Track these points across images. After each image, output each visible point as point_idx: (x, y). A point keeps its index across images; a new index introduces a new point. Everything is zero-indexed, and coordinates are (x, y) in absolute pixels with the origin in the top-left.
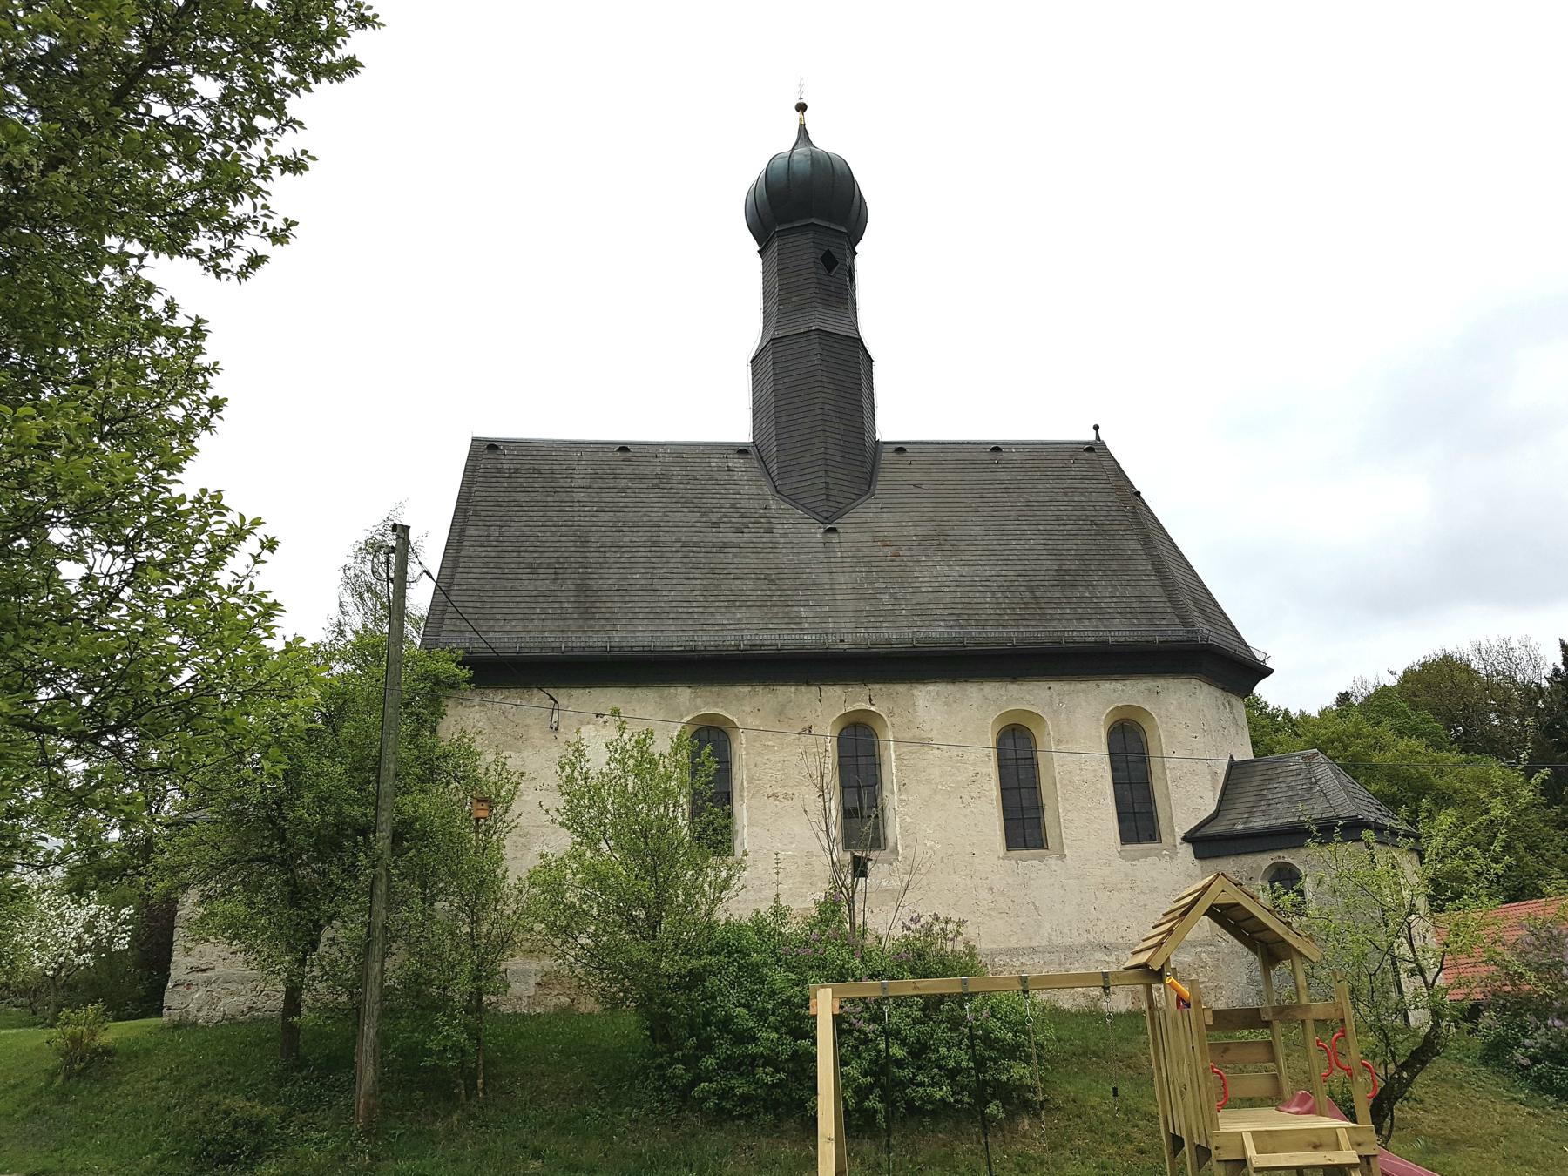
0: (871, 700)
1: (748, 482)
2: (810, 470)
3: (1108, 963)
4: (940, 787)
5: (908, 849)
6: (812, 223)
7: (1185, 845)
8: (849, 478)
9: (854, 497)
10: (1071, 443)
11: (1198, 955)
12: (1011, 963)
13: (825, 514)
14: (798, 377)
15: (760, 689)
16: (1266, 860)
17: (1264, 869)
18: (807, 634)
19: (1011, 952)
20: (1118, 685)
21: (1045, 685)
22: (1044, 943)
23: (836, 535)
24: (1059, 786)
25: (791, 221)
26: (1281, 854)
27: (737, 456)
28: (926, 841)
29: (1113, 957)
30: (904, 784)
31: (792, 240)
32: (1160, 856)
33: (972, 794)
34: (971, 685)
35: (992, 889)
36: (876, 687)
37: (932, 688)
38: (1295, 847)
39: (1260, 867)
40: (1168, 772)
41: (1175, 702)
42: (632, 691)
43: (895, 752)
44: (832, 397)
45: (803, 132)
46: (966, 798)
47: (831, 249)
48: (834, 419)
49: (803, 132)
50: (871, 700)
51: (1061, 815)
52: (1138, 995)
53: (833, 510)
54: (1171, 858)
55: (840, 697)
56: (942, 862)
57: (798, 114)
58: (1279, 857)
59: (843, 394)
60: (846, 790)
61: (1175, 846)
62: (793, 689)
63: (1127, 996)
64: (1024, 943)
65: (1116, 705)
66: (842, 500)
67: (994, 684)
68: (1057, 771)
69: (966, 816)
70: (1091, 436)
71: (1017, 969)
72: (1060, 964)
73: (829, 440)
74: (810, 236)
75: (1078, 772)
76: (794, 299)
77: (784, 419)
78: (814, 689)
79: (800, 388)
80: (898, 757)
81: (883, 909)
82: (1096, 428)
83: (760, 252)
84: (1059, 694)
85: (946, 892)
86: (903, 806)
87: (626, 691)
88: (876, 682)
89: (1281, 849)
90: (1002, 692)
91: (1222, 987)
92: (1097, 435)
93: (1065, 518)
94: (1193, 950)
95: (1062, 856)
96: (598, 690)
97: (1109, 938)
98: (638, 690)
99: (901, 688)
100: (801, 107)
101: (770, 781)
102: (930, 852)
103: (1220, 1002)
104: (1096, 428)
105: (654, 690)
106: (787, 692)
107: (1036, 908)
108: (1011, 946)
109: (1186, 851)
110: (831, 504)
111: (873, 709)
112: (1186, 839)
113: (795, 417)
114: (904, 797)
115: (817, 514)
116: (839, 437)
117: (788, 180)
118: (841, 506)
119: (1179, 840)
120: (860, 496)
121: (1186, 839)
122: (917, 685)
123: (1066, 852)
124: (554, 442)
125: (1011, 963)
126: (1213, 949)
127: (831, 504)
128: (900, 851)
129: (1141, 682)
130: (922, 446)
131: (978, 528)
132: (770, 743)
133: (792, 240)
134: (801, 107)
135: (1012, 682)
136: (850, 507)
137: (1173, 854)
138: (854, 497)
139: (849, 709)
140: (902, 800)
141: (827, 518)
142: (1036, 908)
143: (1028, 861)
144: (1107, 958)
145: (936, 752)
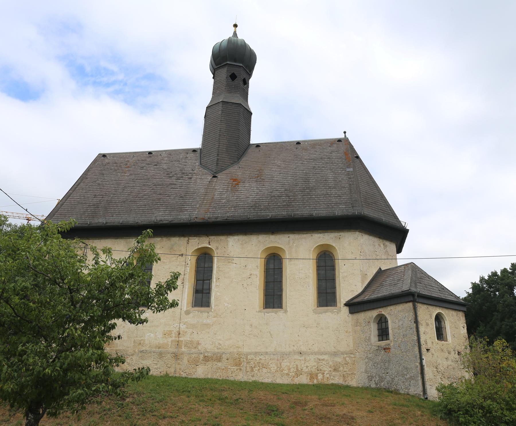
0: (209, 243)
1: (194, 161)
2: (212, 155)
3: (300, 360)
4: (234, 280)
5: (217, 307)
6: (227, 64)
7: (345, 307)
8: (229, 157)
9: (230, 164)
10: (332, 139)
11: (345, 358)
12: (255, 358)
13: (215, 171)
14: (214, 120)
15: (165, 239)
16: (374, 313)
17: (374, 317)
18: (184, 217)
19: (256, 354)
20: (321, 235)
21: (287, 236)
22: (273, 350)
23: (216, 178)
24: (288, 280)
25: (221, 64)
26: (380, 310)
27: (192, 153)
28: (225, 303)
29: (303, 358)
30: (219, 279)
31: (220, 71)
32: (332, 312)
33: (248, 283)
34: (253, 236)
35: (251, 325)
36: (212, 238)
37: (236, 238)
38: (386, 306)
39: (372, 316)
40: (341, 274)
41: (347, 243)
42: (116, 240)
43: (217, 265)
44: (225, 126)
45: (235, 34)
46: (245, 285)
47: (235, 72)
48: (224, 134)
49: (235, 34)
50: (209, 243)
51: (288, 293)
52: (313, 375)
53: (219, 169)
54: (338, 313)
55: (196, 242)
56: (231, 313)
57: (233, 28)
58: (380, 312)
59: (230, 125)
60: (198, 281)
61: (340, 308)
62: (178, 239)
63: (307, 376)
64: (263, 350)
65: (319, 244)
66: (224, 165)
67: (264, 235)
68: (288, 273)
69: (244, 293)
70: (342, 136)
71: (258, 361)
72: (278, 360)
73: (221, 142)
74: (226, 68)
75: (298, 274)
76: (218, 92)
77: (207, 136)
78: (186, 239)
79: (214, 124)
80: (218, 267)
81: (203, 332)
82: (345, 132)
83: (213, 78)
84: (293, 239)
85: (231, 326)
86: (217, 288)
87: (113, 240)
88: (212, 235)
89: (380, 307)
90: (267, 239)
91: (355, 374)
92: (345, 136)
93: (317, 167)
94: (342, 356)
95: (286, 312)
96: (103, 240)
97: (303, 349)
98: (118, 240)
99: (223, 238)
100: (235, 26)
101: (163, 276)
102: (226, 308)
103: (353, 381)
104: (345, 132)
105: (124, 240)
106: (175, 240)
107: (271, 334)
108: (257, 351)
109: (346, 309)
110: (218, 167)
111: (210, 246)
112: (346, 305)
113: (210, 135)
114: (218, 284)
115: (212, 171)
116: (226, 141)
117: (220, 49)
118: (223, 167)
119: (342, 305)
120: (233, 163)
121: (346, 305)
122: (230, 236)
123: (288, 310)
124: (127, 153)
125: (255, 358)
126: (352, 356)
127: (218, 167)
128: (213, 307)
129: (332, 234)
130: (268, 145)
131: (277, 173)
132: (165, 261)
133: (220, 71)
134: (235, 26)
135: (272, 234)
136: (227, 168)
137: (340, 311)
138: (230, 164)
139: (200, 247)
140: (217, 286)
141: (215, 173)
142: (271, 334)
143: (272, 314)
144: (300, 358)
145: (235, 265)
